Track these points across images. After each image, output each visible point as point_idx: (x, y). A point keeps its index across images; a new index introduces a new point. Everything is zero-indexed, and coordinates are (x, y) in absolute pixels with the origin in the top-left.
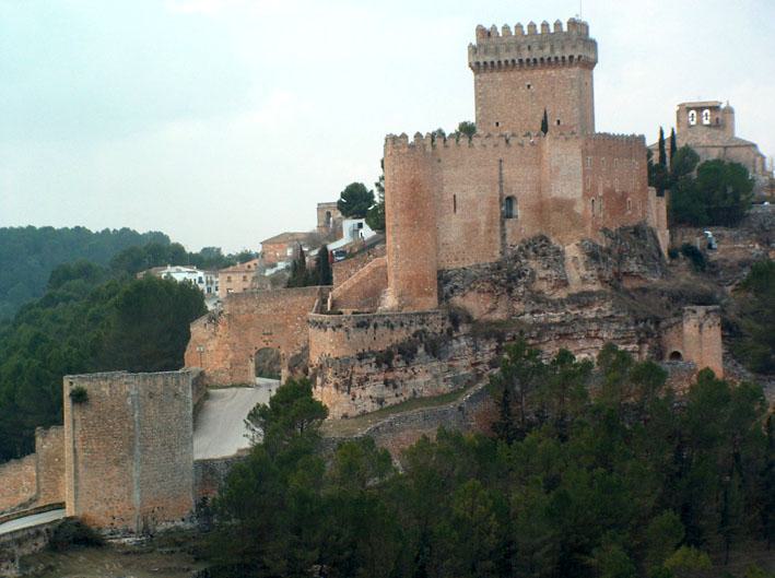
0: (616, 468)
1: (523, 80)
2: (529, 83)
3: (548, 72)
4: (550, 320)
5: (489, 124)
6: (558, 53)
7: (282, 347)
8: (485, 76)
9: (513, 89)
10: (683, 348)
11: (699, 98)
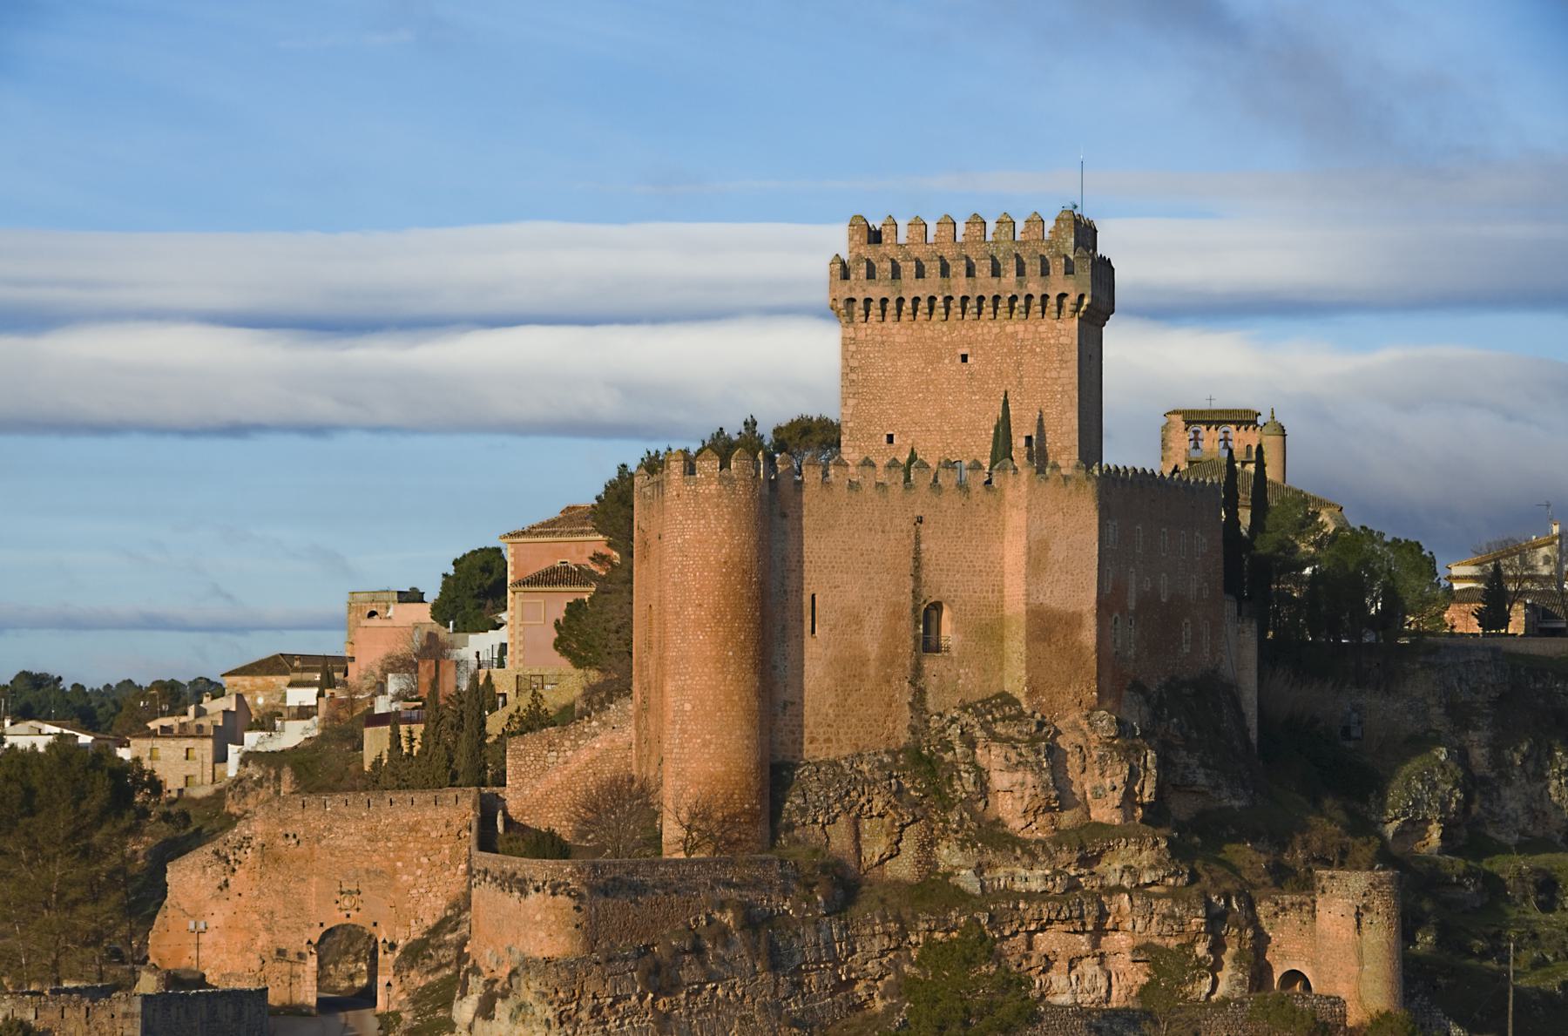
0: (620, 634)
1: (951, 342)
2: (965, 351)
3: (1009, 329)
4: (1019, 886)
5: (871, 436)
6: (1034, 287)
7: (381, 925)
8: (870, 330)
9: (928, 363)
10: (1312, 962)
11: (989, 442)
